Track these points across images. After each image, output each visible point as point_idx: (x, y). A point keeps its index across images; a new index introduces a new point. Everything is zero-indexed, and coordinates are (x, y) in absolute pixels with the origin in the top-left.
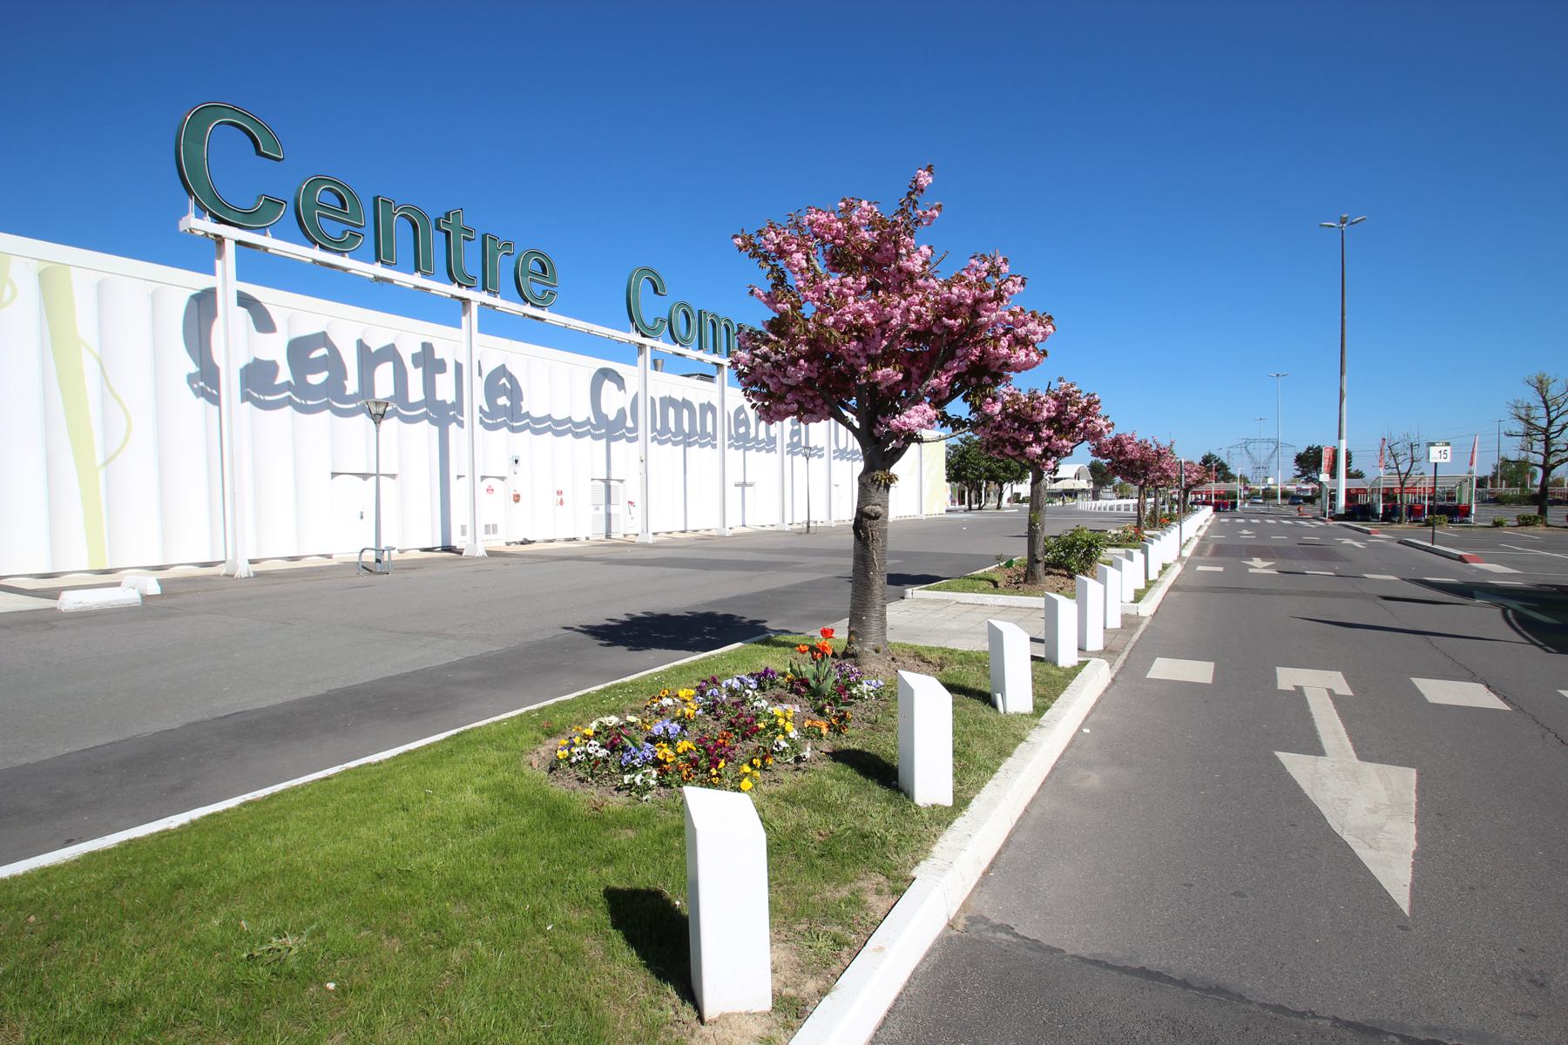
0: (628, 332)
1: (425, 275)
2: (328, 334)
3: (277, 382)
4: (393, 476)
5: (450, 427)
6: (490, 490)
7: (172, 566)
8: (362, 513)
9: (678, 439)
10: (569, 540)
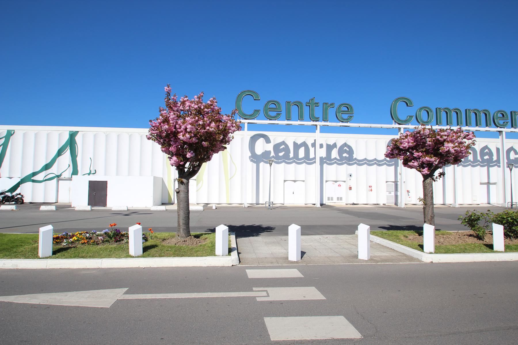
0: (392, 124)
1: (489, 127)
2: (285, 141)
3: (494, 160)
4: (495, 184)
5: (324, 165)
6: (339, 185)
7: (222, 204)
8: (293, 192)
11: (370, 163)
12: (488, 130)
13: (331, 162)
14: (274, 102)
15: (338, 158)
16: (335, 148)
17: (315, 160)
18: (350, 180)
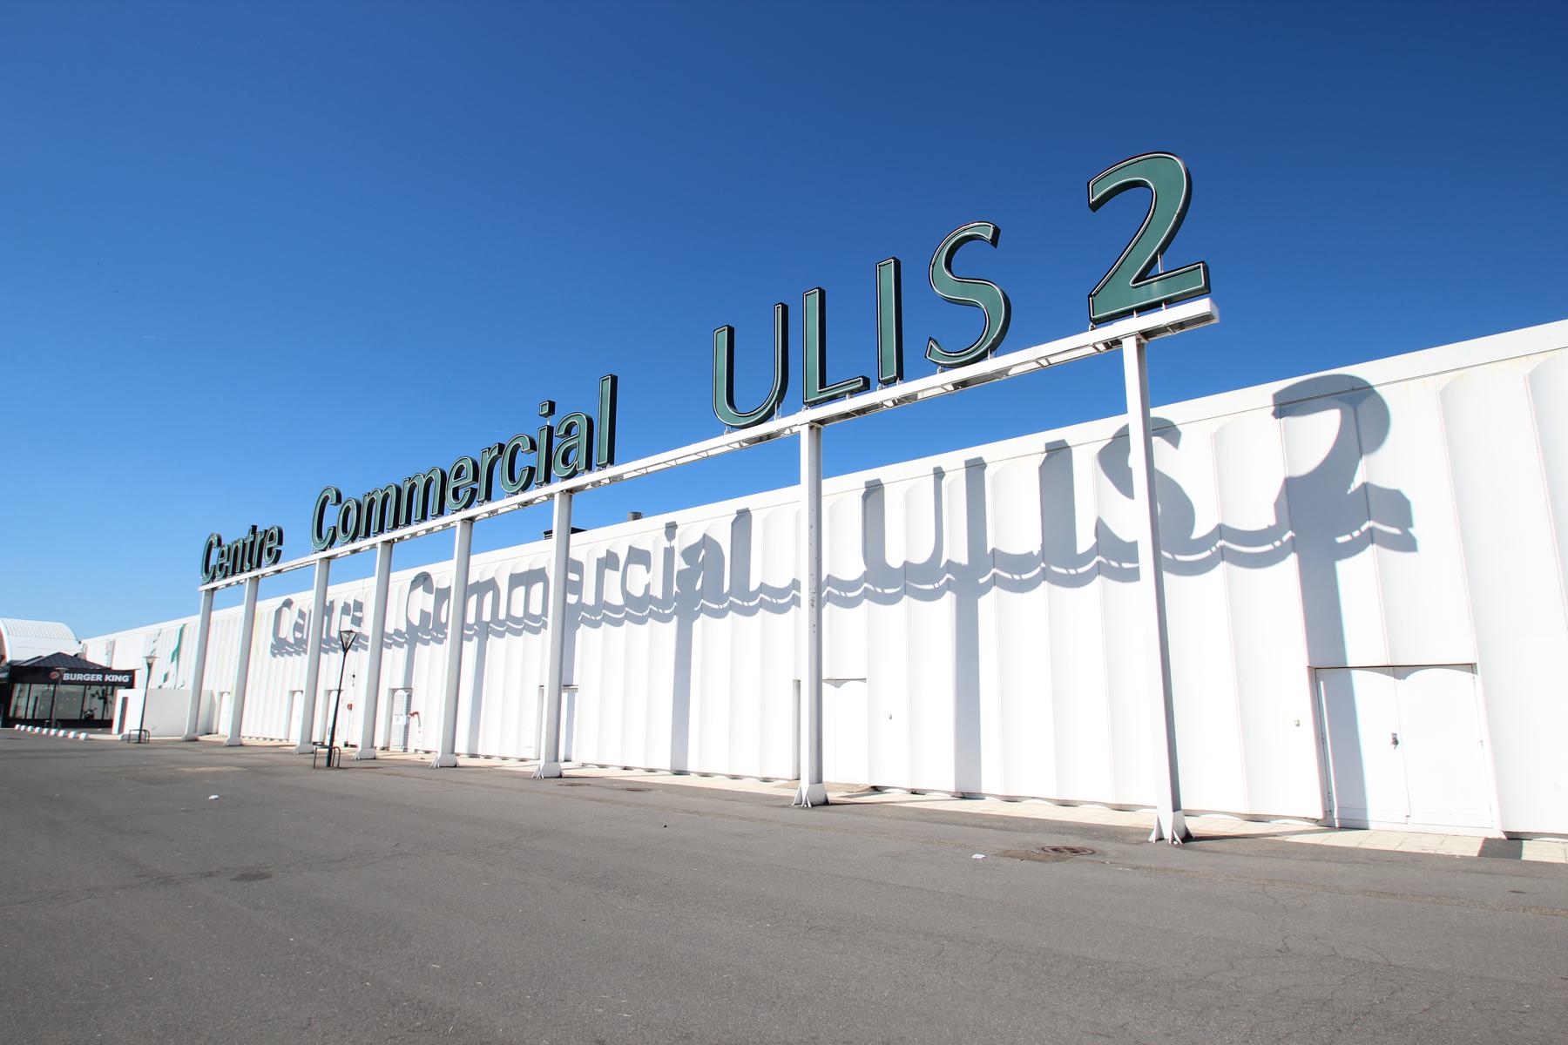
7: (1278, 817)
13: (1072, 572)
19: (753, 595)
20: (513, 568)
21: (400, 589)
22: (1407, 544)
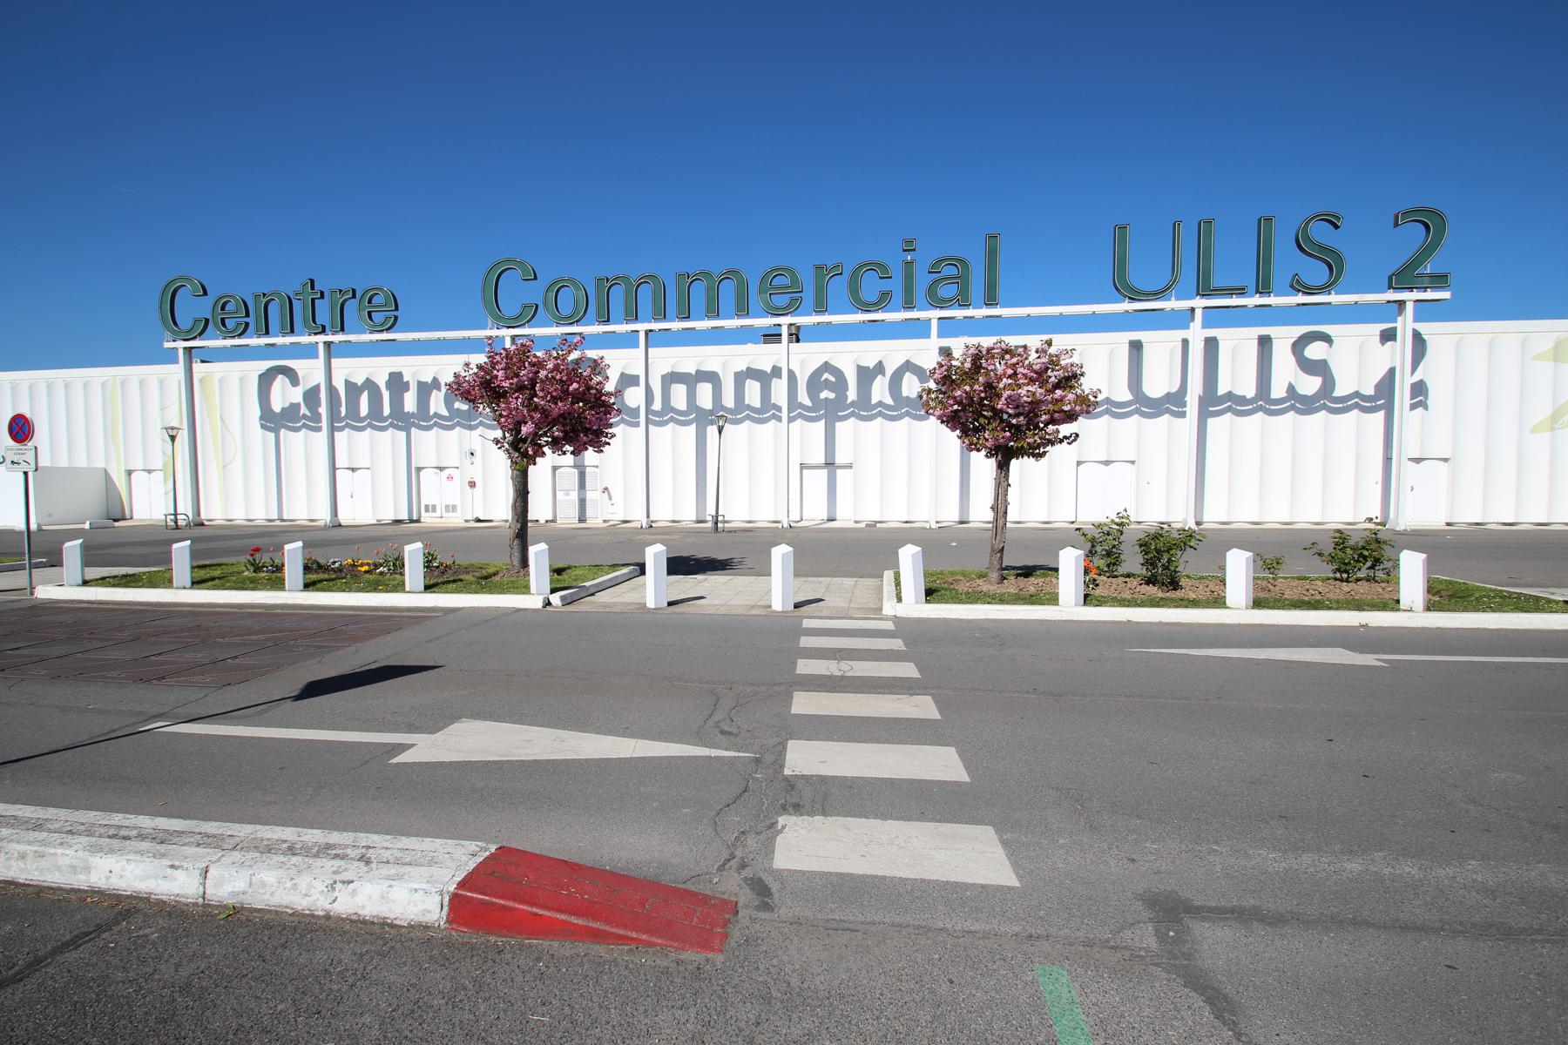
4: (850, 466)
6: (450, 478)
9: (691, 417)
10: (906, 522)
11: (1272, 407)
12: (880, 319)
14: (779, 271)
15: (890, 401)
16: (880, 377)
17: (791, 415)
18: (472, 464)
19: (431, 418)
20: (672, 367)
21: (241, 379)
22: (1426, 408)
